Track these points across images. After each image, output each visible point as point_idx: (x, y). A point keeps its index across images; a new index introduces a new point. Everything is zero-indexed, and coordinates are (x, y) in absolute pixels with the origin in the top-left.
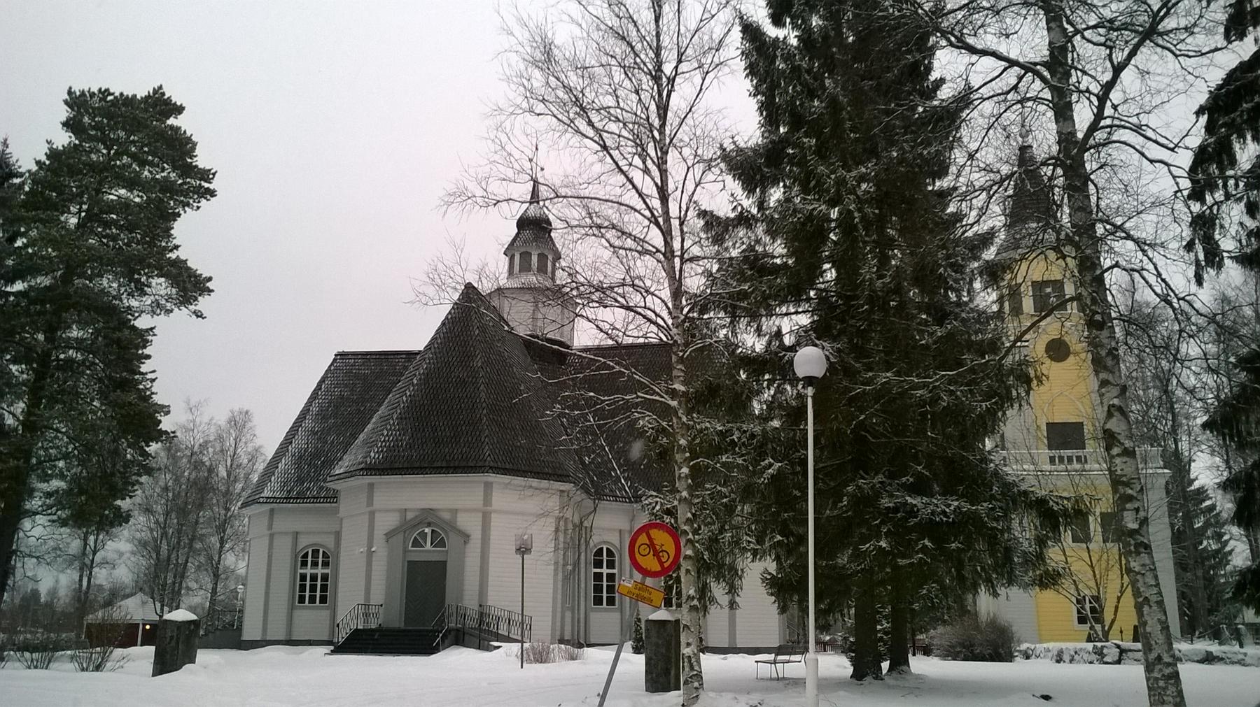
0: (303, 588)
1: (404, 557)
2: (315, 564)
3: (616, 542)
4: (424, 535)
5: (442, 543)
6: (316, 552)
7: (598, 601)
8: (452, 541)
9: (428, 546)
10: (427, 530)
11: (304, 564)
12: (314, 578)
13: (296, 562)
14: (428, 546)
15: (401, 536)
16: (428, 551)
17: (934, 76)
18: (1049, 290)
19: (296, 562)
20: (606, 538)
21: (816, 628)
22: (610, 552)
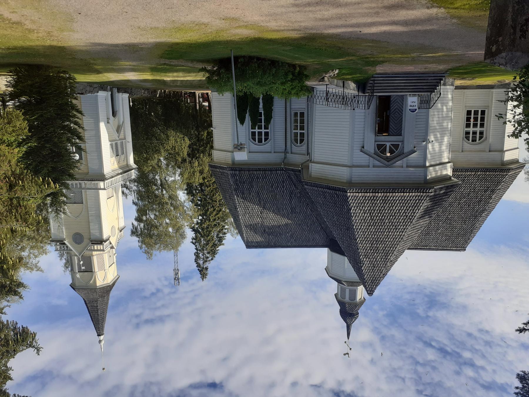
0: (296, 121)
1: (404, 138)
2: (474, 133)
3: (293, 146)
4: (391, 152)
5: (379, 147)
6: (474, 140)
7: (302, 114)
8: (371, 147)
9: (388, 144)
10: (388, 155)
11: (481, 133)
12: (475, 125)
13: (486, 134)
14: (388, 144)
15: (406, 150)
16: (387, 140)
17: (5, 323)
18: (83, 268)
19: (486, 134)
20: (299, 149)
21: (380, 96)
22: (254, 139)
